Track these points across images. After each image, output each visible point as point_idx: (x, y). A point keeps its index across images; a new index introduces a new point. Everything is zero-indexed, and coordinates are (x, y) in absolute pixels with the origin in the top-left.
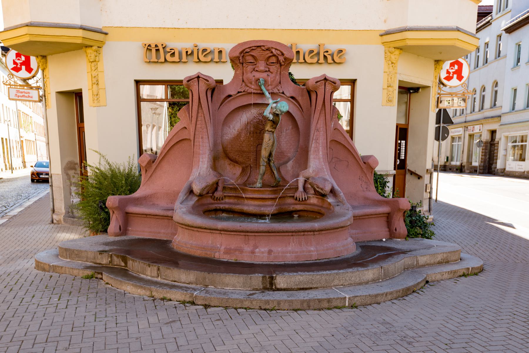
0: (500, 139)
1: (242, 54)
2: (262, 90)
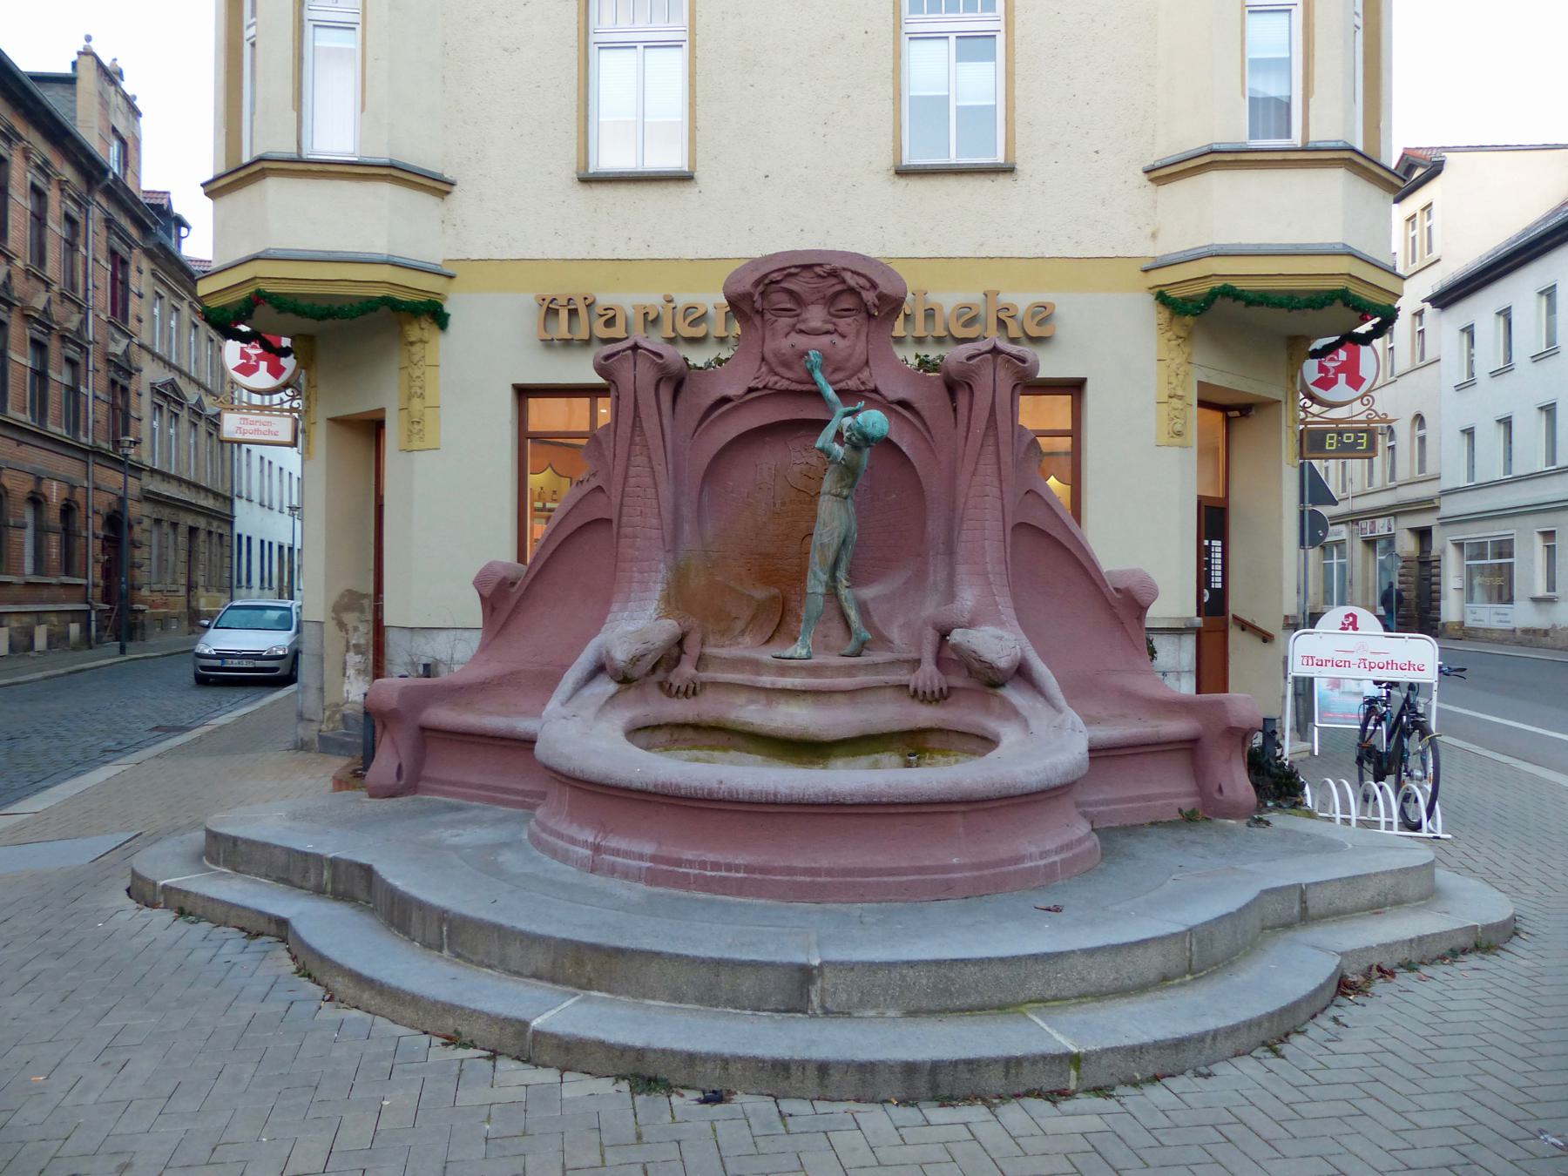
0: (1443, 551)
1: (761, 288)
2: (815, 383)
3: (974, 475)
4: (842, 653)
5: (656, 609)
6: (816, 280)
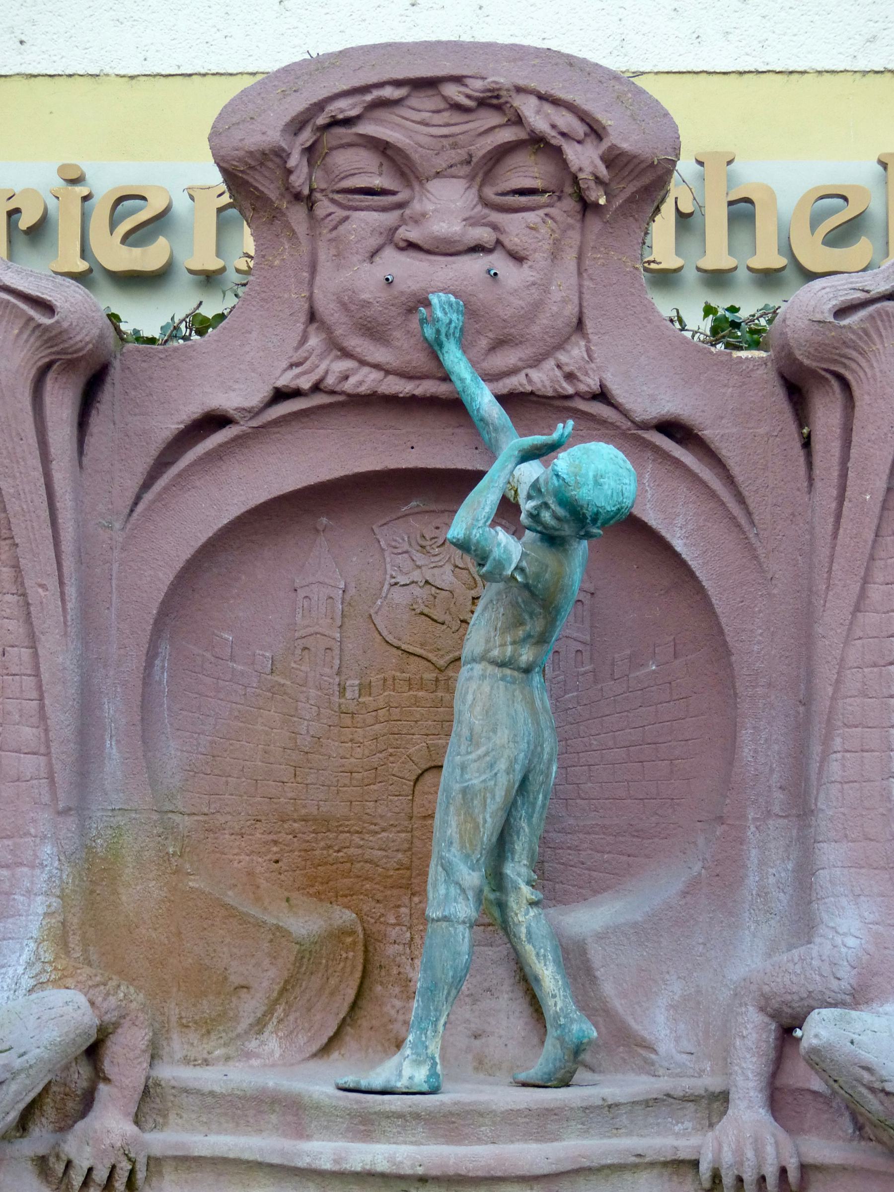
1: (307, 137)
2: (446, 378)
3: (857, 609)
4: (522, 1076)
5: (30, 964)
6: (446, 117)
